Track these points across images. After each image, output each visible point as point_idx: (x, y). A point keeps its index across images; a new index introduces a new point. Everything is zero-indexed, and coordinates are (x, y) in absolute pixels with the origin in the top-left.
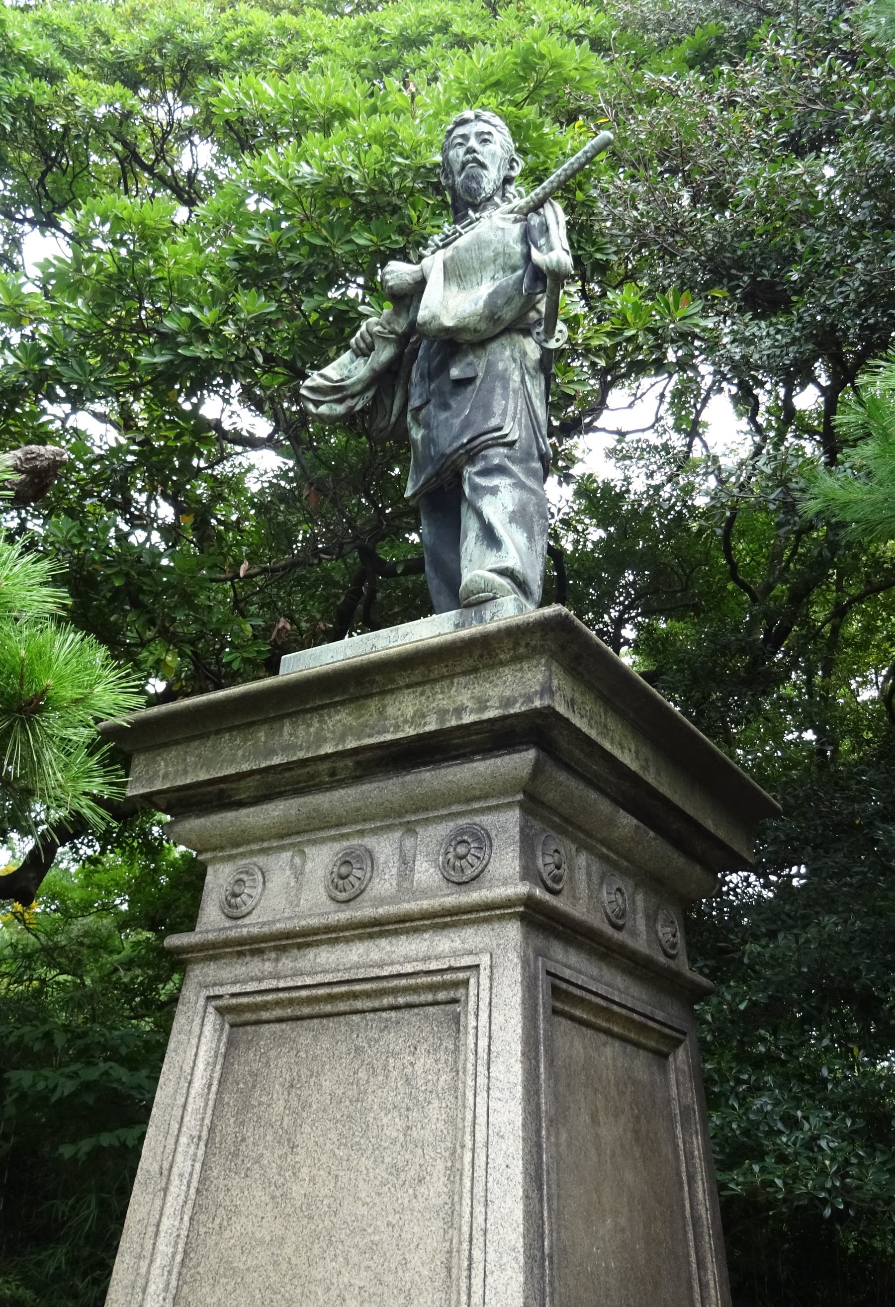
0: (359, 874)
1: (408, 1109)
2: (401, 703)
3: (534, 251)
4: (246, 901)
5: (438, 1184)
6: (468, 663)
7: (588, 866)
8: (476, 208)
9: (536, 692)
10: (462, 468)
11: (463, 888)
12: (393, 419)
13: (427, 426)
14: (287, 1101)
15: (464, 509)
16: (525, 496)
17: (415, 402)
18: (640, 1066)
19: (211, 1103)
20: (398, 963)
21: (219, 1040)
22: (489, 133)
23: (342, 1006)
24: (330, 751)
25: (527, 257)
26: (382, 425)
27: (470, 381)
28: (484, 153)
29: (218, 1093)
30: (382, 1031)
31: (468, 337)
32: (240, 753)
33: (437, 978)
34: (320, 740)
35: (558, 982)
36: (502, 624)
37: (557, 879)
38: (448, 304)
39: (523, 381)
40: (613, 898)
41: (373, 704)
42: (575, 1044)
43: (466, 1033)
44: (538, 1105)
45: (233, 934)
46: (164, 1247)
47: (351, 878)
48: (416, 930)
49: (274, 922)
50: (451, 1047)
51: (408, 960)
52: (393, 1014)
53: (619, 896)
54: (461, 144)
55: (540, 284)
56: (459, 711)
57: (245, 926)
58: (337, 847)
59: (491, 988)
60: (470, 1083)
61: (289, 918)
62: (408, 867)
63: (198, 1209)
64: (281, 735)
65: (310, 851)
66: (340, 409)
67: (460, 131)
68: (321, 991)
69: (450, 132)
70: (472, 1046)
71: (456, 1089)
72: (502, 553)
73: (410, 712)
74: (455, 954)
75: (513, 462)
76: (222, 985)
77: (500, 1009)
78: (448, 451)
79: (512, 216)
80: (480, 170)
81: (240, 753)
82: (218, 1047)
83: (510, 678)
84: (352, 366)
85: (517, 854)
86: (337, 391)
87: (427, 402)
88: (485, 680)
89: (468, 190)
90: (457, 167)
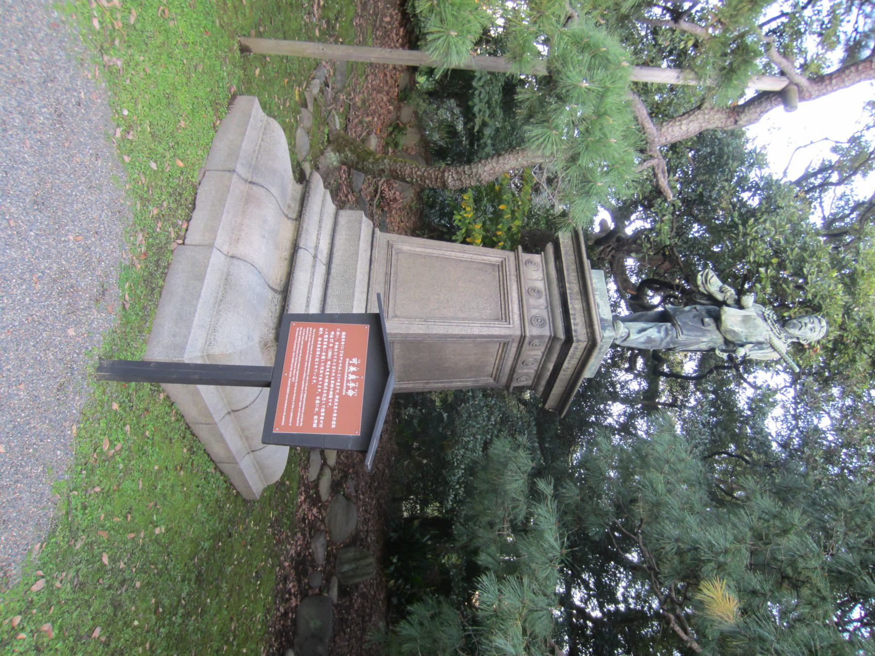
5: (462, 315)
16: (658, 342)
18: (490, 369)
25: (751, 343)
38: (731, 317)
41: (579, 297)
42: (494, 348)
45: (521, 263)
46: (448, 253)
56: (575, 319)
62: (538, 306)
63: (456, 260)
66: (699, 283)
77: (499, 330)
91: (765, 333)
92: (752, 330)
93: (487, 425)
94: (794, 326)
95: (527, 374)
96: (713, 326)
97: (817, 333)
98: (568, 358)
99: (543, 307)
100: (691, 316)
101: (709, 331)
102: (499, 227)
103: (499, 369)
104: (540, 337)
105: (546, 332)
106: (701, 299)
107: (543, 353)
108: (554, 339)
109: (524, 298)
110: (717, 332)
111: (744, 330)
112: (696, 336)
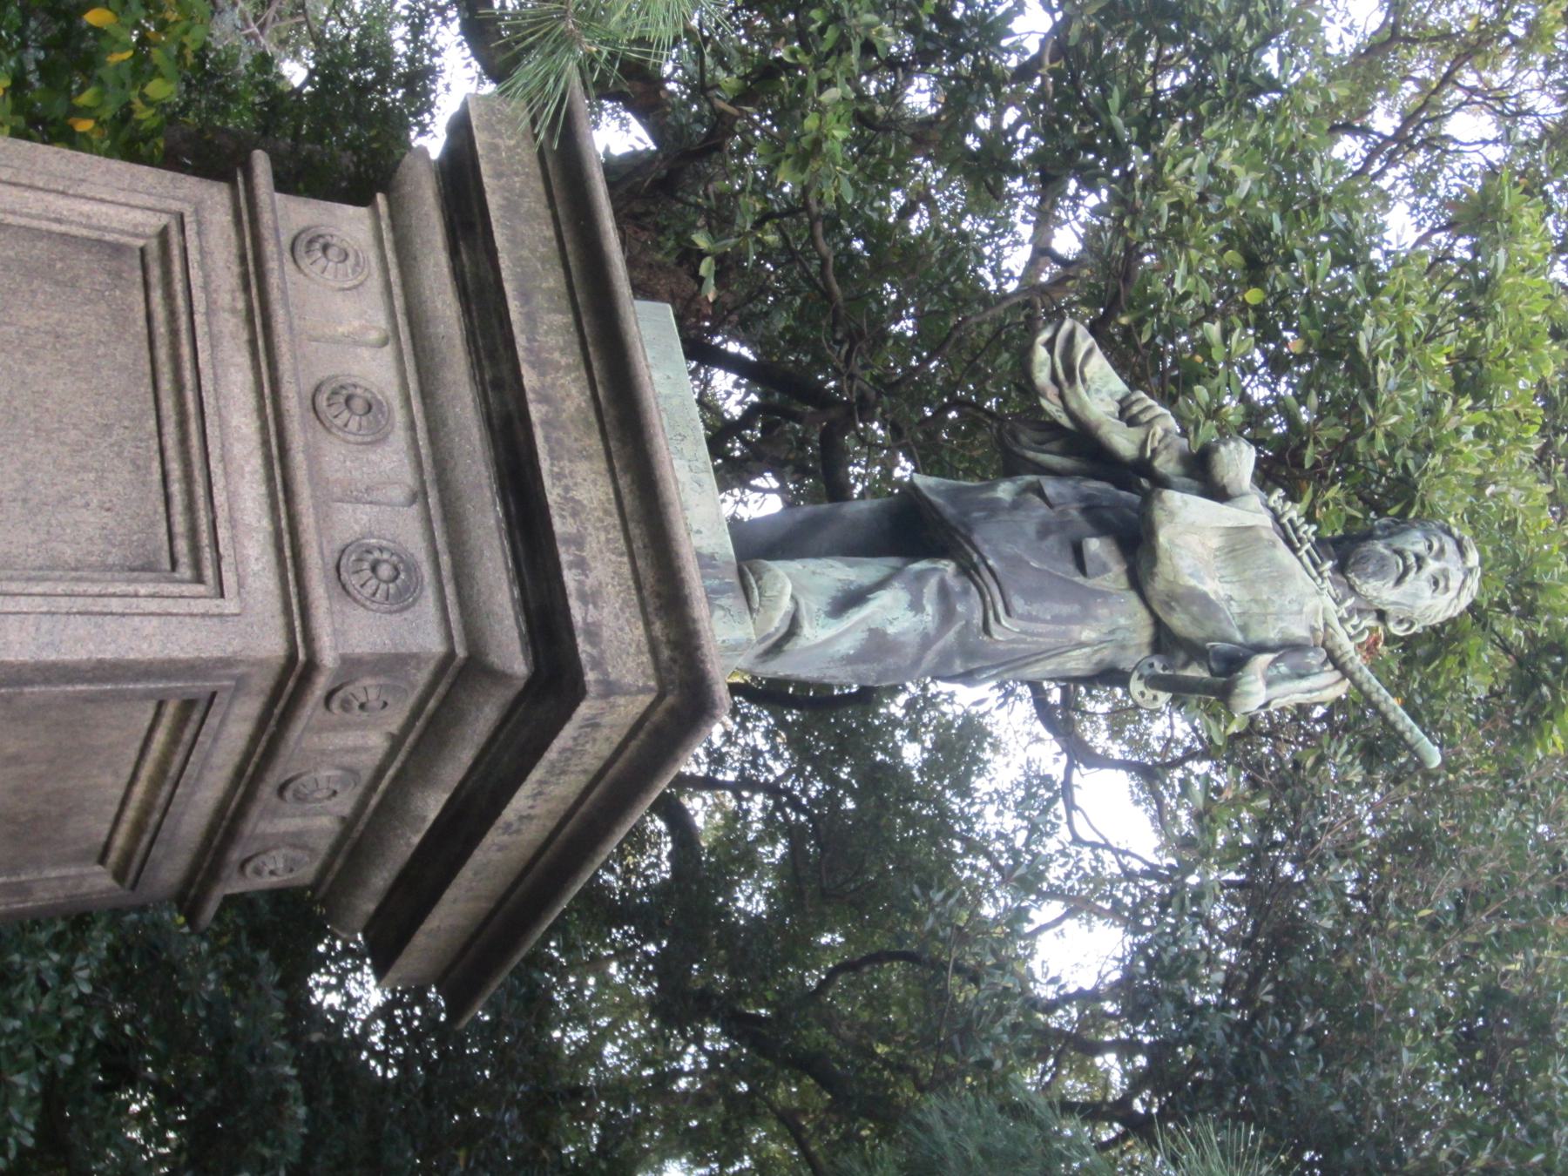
0: (353, 425)
1: (25, 501)
2: (594, 482)
3: (1269, 657)
4: (315, 264)
6: (649, 578)
7: (366, 749)
8: (1341, 569)
9: (607, 674)
10: (952, 558)
11: (333, 573)
12: (1030, 454)
13: (1015, 505)
14: (37, 330)
15: (893, 561)
16: (911, 651)
17: (1051, 487)
19: (35, 223)
20: (228, 483)
21: (122, 232)
22: (1447, 589)
23: (168, 405)
24: (526, 382)
25: (1261, 648)
26: (1024, 438)
27: (1081, 566)
28: (1418, 583)
29: (50, 233)
30: (133, 462)
32: (526, 253)
33: (205, 539)
34: (541, 366)
35: (200, 708)
36: (703, 626)
37: (346, 706)
38: (1190, 530)
39: (1081, 645)
40: (323, 784)
41: (595, 443)
42: (125, 726)
43: (130, 581)
44: (31, 682)
45: (270, 248)
47: (346, 414)
48: (274, 508)
49: (286, 306)
50: (110, 560)
51: (232, 497)
52: (157, 477)
53: (325, 793)
54: (1430, 547)
56: (581, 564)
57: (281, 265)
58: (393, 395)
59: (192, 615)
60: (60, 589)
61: (291, 328)
62: (370, 489)
64: (549, 311)
65: (388, 352)
66: (1042, 377)
67: (1450, 546)
68: (188, 375)
69: (1449, 532)
70: (111, 590)
71: (52, 568)
72: (823, 619)
73: (580, 494)
74: (239, 563)
75: (959, 633)
76: (199, 234)
77: (161, 628)
78: (976, 538)
80: (1394, 576)
81: (526, 253)
82: (113, 231)
83: (627, 638)
84: (1104, 395)
85: (379, 649)
86: (1070, 372)
87: (1051, 506)
88: (624, 601)
89: (1364, 559)
90: (1398, 543)
91: (1311, 604)
92: (1265, 591)
93: (58, 1011)
94: (1381, 571)
95: (296, 841)
96: (1114, 576)
97: (1452, 593)
98: (537, 774)
99: (398, 494)
100: (1031, 528)
101: (1104, 595)
102: (86, 99)
103: (150, 825)
104: (391, 664)
105: (423, 633)
106: (1040, 446)
107: (396, 742)
108: (464, 672)
109: (297, 441)
110: (1133, 599)
111: (1235, 591)
112: (1056, 619)
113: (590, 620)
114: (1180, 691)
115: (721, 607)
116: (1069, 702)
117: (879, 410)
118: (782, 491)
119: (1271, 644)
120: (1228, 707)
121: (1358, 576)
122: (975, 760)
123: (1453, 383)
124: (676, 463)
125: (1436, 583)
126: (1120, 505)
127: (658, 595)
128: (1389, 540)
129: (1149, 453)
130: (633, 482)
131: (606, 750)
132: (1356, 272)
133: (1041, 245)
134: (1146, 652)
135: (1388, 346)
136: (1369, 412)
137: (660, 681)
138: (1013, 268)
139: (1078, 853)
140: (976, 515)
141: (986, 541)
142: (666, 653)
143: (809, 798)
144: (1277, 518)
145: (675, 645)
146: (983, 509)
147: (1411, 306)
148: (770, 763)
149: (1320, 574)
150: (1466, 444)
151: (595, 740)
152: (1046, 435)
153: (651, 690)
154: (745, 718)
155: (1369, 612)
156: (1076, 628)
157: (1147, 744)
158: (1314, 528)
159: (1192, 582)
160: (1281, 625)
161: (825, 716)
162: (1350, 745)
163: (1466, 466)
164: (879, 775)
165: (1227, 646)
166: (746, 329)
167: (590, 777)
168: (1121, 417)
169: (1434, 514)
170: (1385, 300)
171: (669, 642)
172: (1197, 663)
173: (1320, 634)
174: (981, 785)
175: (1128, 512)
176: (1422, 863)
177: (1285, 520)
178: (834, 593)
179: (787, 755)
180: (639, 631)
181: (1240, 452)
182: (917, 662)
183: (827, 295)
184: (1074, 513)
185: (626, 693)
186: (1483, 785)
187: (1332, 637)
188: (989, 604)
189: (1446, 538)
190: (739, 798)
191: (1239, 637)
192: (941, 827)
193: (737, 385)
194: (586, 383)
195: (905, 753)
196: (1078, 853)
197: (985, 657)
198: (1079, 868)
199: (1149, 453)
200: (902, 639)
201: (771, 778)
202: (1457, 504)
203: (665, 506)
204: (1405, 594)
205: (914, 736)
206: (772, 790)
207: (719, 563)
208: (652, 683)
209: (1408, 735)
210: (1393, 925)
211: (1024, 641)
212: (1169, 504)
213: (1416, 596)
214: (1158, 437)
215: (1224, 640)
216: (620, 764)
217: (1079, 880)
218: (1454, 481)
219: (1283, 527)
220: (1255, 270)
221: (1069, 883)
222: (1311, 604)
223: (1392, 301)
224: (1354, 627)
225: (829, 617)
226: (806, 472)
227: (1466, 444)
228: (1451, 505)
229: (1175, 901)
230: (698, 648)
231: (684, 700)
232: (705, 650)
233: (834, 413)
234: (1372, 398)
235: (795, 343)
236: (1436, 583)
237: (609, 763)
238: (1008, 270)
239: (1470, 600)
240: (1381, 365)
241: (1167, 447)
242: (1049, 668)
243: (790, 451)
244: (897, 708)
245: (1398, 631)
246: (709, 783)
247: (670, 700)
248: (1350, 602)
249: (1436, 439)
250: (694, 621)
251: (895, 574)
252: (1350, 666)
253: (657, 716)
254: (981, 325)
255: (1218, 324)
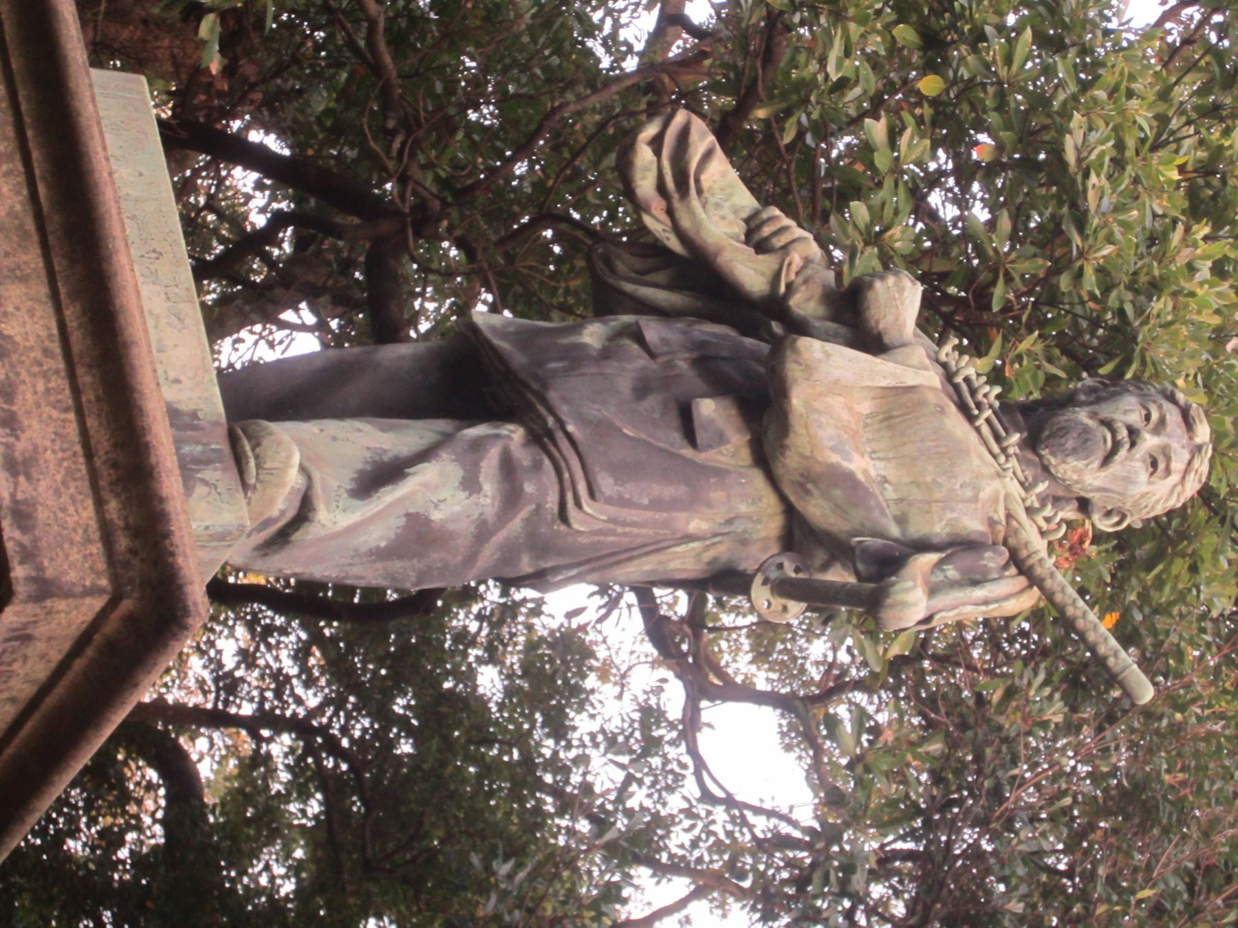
2: (31, 313)
3: (933, 557)
6: (102, 441)
8: (1032, 443)
9: (40, 568)
12: (629, 287)
13: (606, 354)
15: (442, 425)
16: (463, 543)
17: (653, 331)
22: (1168, 472)
25: (924, 546)
26: (621, 267)
27: (690, 435)
28: (1131, 463)
31: (771, 435)
38: (831, 386)
39: (689, 538)
41: (32, 259)
54: (1148, 418)
55: (873, 569)
66: (645, 185)
67: (1173, 416)
69: (1172, 399)
78: (553, 396)
79: (1001, 515)
84: (725, 211)
86: (682, 180)
87: (652, 355)
88: (69, 472)
89: (1063, 432)
90: (1106, 411)
91: (989, 489)
97: (1175, 478)
100: (625, 385)
101: (720, 473)
106: (640, 276)
110: (758, 480)
112: (657, 504)
113: (20, 496)
114: (822, 601)
115: (206, 483)
116: (696, 620)
117: (445, 223)
118: (321, 327)
119: (935, 540)
120: (877, 621)
121: (1053, 454)
122: (576, 690)
123: (1186, 204)
124: (145, 291)
125: (1154, 464)
126: (742, 358)
127: (115, 465)
128: (1095, 408)
129: (782, 289)
130: (84, 313)
131: (41, 672)
132: (1065, 57)
133: (673, 11)
134: (775, 549)
135: (1102, 154)
136: (1077, 240)
137: (115, 578)
138: (632, 40)
139: (709, 813)
140: (553, 365)
141: (565, 400)
142: (123, 543)
143: (352, 741)
144: (949, 376)
145: (135, 532)
146: (560, 359)
147: (1134, 103)
148: (299, 691)
149: (1004, 450)
150: (1201, 284)
151: (25, 658)
152: (649, 262)
153: (99, 591)
154: (269, 630)
155: (1068, 500)
156: (680, 516)
157: (802, 671)
158: (998, 390)
159: (835, 458)
160: (949, 515)
161: (379, 629)
162: (1049, 675)
163: (1199, 312)
164: (443, 709)
165: (879, 542)
166: (273, 111)
167: (21, 706)
168: (747, 242)
169: (1157, 375)
170: (1101, 94)
171: (127, 527)
172: (837, 564)
173: (1001, 529)
174: (582, 724)
175: (753, 364)
176: (1143, 829)
177: (959, 379)
178: (360, 466)
179: (323, 682)
180: (88, 512)
181: (901, 290)
182: (471, 559)
183: (377, 68)
184: (683, 365)
185: (67, 594)
186: (1217, 727)
187: (1016, 532)
188: (567, 484)
189: (1167, 405)
190: (259, 739)
191: (895, 531)
192: (525, 776)
193: (259, 186)
194: (22, 179)
195: (480, 680)
196: (709, 813)
197: (560, 552)
198: (710, 833)
199: (782, 289)
200: (451, 527)
201: (301, 712)
202: (1188, 362)
203: (126, 345)
204: (1115, 478)
205: (493, 656)
206: (300, 727)
207: (202, 423)
208: (104, 582)
209: (1111, 661)
210: (1101, 909)
211: (614, 533)
212: (806, 356)
213: (1128, 480)
214: (794, 268)
215: (875, 534)
216: (60, 690)
217: (709, 849)
218: (1184, 331)
219: (956, 387)
220: (934, 48)
221: (696, 853)
222: (989, 489)
223: (1110, 96)
224: (1047, 520)
225: (362, 498)
226: (357, 306)
227: (1201, 284)
228: (1180, 362)
229: (817, 877)
230: (167, 535)
231: (149, 607)
232: (176, 539)
233: (385, 227)
234: (1081, 221)
235: (338, 130)
236: (1154, 464)
237: (45, 689)
238: (626, 43)
239: (1198, 487)
240: (1093, 179)
241: (806, 281)
242: (647, 568)
243: (330, 275)
244: (465, 619)
245: (1106, 526)
246: (218, 719)
247: (127, 605)
248: (1042, 487)
249: (1162, 278)
250: (161, 500)
251: (445, 440)
252: (1038, 571)
253: (112, 624)
254: (583, 112)
255: (883, 121)
